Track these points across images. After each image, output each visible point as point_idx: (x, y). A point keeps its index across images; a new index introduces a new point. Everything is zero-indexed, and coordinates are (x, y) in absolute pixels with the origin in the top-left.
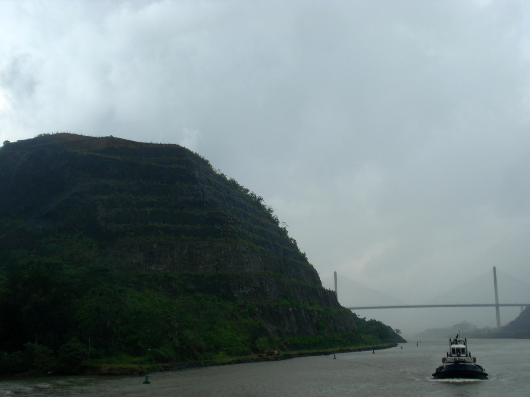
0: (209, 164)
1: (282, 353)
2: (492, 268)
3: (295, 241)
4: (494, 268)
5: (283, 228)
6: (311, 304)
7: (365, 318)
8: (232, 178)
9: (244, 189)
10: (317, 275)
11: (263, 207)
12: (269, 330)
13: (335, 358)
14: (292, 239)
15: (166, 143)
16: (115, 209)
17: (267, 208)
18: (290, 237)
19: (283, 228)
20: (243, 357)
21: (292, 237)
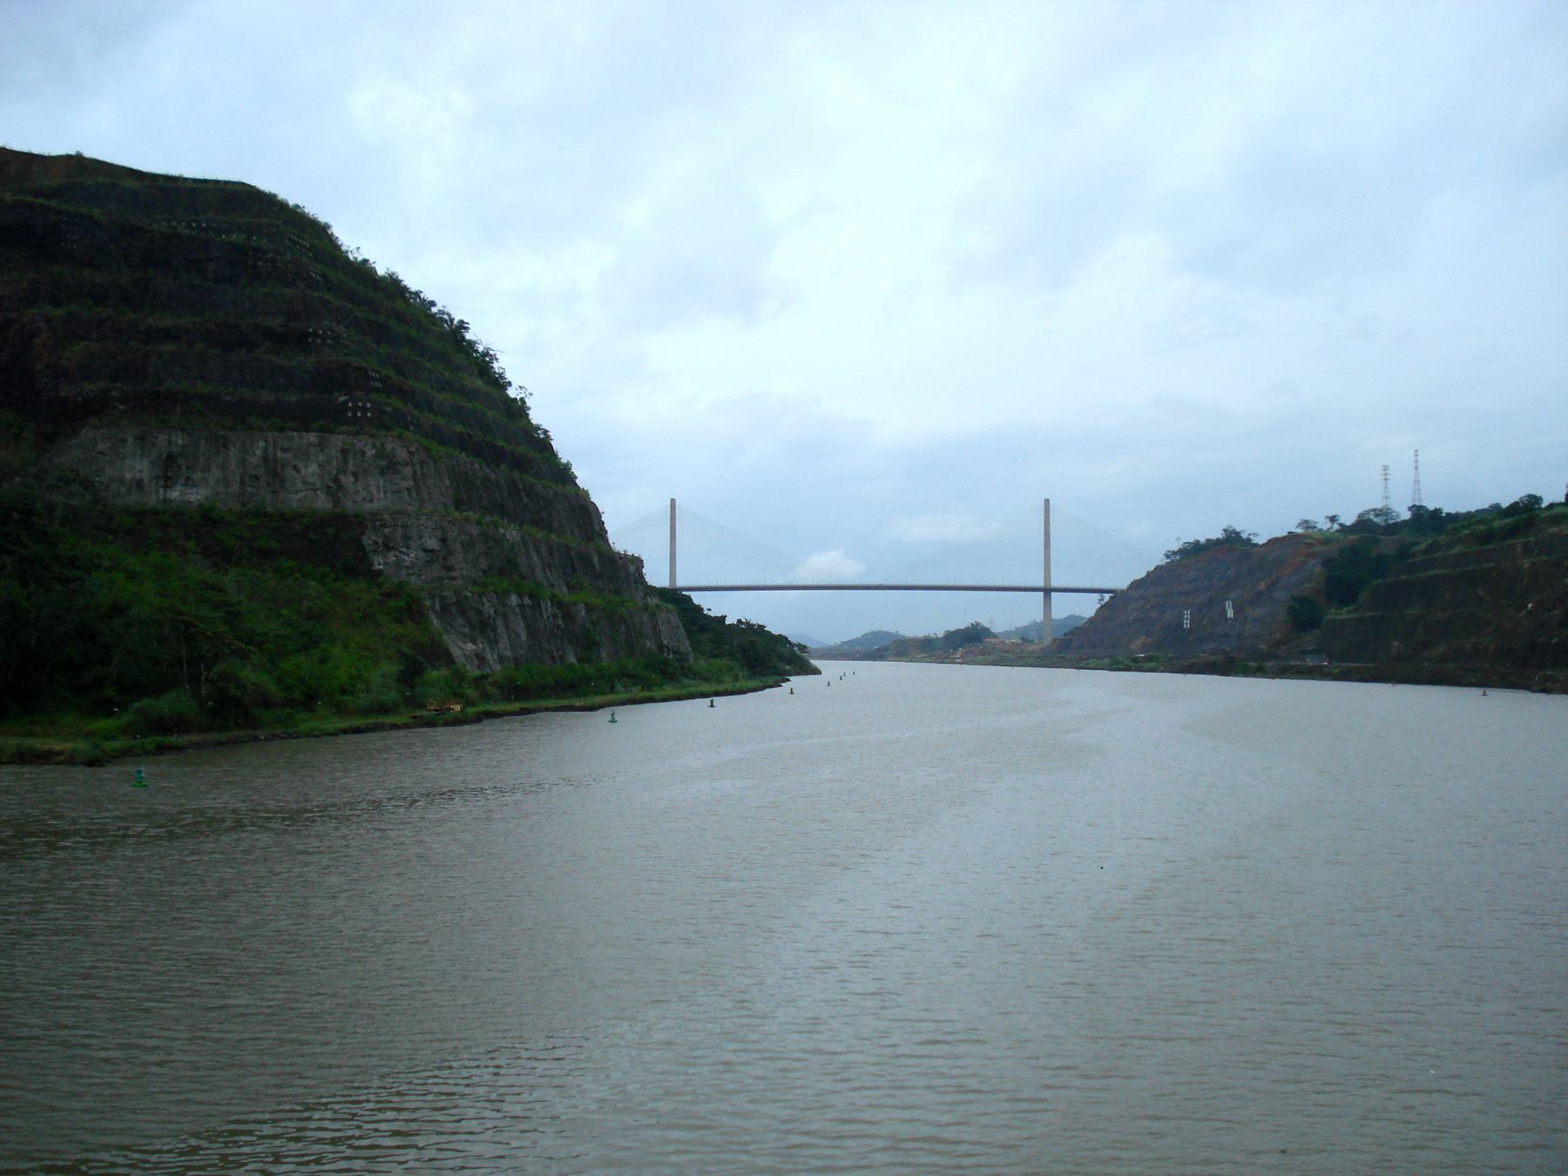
0: (332, 234)
3: (546, 432)
4: (673, 501)
5: (518, 399)
6: (571, 588)
8: (392, 270)
9: (424, 300)
10: (599, 515)
11: (471, 344)
13: (613, 721)
15: (219, 179)
16: (82, 344)
17: (481, 349)
18: (534, 422)
19: (518, 399)
21: (540, 423)
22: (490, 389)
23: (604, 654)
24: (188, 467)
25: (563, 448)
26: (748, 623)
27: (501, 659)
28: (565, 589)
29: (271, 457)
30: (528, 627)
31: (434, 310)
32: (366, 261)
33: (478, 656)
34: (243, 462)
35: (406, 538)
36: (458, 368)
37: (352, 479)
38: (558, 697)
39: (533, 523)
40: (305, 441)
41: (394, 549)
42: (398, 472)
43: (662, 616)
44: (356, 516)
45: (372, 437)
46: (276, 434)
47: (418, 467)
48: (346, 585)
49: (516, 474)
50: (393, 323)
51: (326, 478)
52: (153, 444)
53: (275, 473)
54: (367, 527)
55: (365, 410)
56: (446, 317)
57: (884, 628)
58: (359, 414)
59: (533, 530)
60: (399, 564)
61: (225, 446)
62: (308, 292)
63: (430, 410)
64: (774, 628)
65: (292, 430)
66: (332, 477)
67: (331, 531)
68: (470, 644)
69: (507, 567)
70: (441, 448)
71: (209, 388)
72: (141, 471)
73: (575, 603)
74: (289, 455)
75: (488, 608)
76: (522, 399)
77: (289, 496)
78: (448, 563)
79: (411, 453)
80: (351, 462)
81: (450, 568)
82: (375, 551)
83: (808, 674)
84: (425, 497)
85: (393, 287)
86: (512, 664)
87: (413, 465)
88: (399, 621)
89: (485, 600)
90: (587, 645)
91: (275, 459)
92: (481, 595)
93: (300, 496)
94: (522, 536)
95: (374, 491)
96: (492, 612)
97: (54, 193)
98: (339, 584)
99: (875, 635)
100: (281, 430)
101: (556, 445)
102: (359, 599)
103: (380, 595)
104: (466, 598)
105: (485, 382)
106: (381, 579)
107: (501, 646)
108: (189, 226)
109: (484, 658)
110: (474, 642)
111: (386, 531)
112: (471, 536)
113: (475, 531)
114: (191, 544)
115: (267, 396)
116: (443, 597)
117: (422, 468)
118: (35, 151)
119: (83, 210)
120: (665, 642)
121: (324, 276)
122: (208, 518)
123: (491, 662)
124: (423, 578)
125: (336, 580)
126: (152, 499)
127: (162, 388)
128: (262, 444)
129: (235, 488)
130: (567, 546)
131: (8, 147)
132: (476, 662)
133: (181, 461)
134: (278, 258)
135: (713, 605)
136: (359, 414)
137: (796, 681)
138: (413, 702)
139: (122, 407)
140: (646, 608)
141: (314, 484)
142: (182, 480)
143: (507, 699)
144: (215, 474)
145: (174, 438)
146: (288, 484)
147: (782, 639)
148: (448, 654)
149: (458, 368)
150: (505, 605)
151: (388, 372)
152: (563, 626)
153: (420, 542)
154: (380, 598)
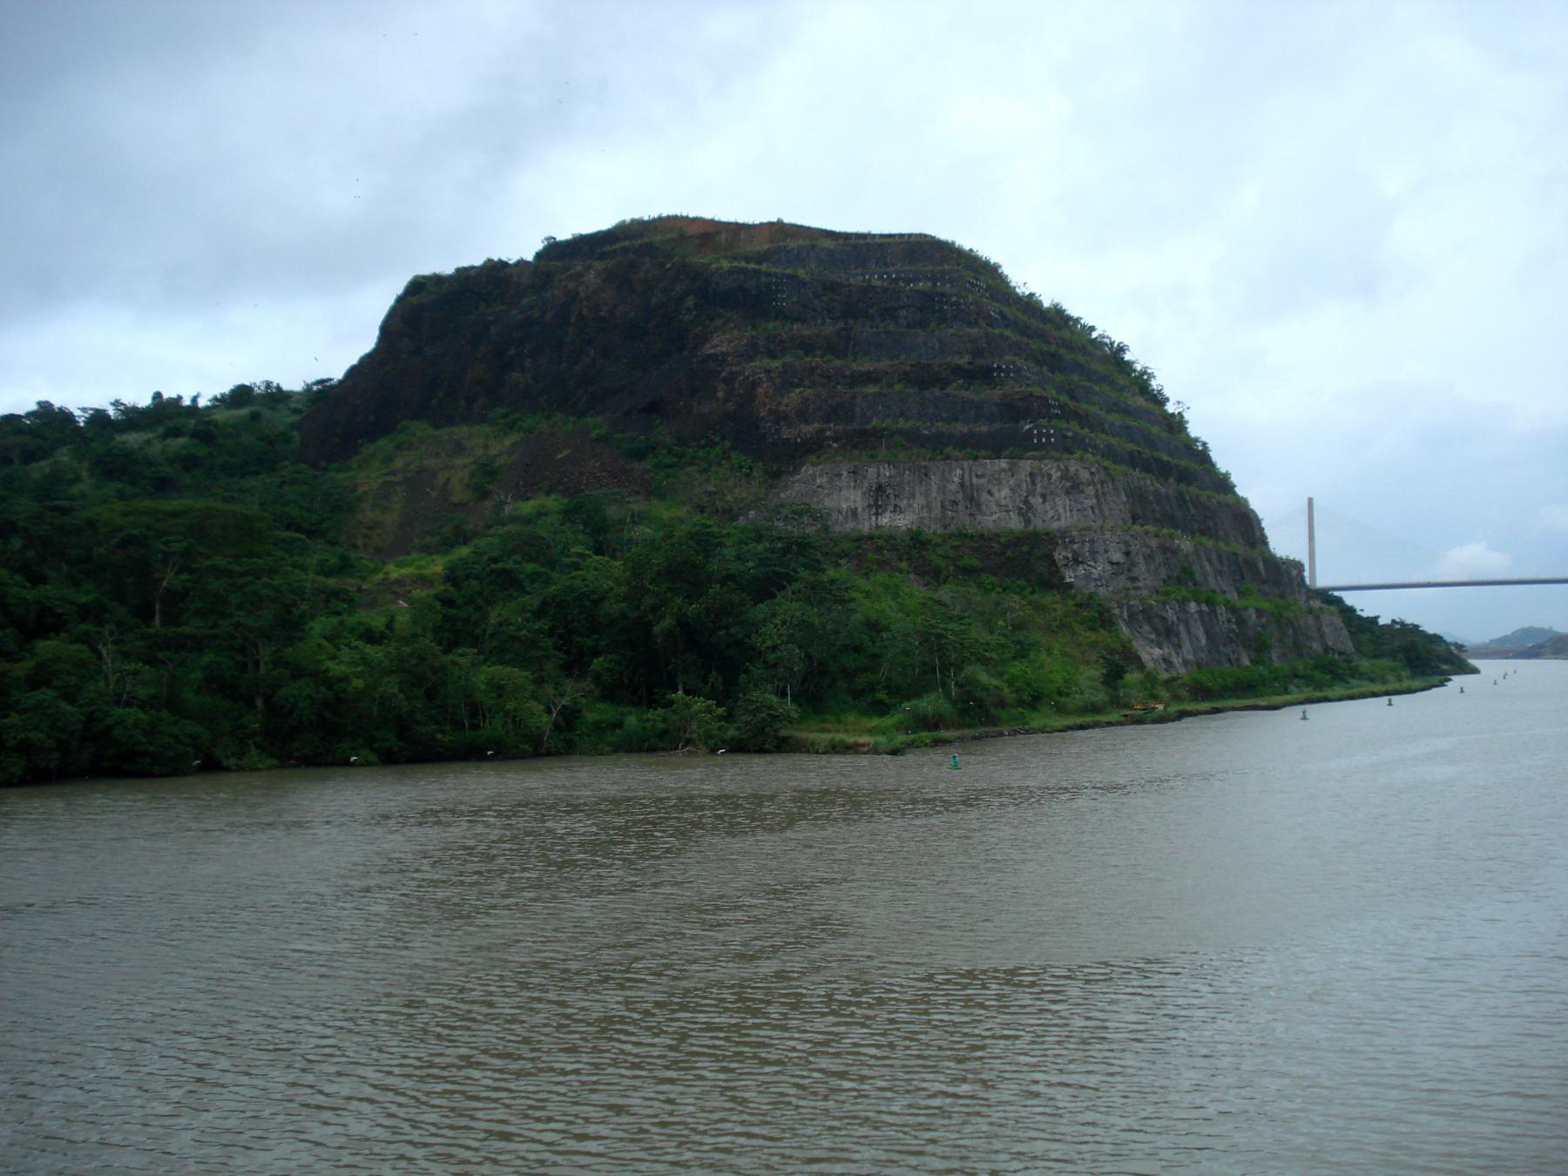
1: (1174, 708)
2: (1306, 503)
3: (1204, 444)
4: (1310, 501)
6: (1241, 594)
7: (1377, 617)
8: (1056, 301)
9: (1084, 326)
10: (1259, 522)
11: (1129, 364)
12: (1145, 657)
13: (1304, 718)
14: (1196, 440)
15: (904, 232)
16: (798, 391)
20: (1088, 719)
21: (1198, 436)
22: (1151, 406)
23: (1274, 656)
24: (896, 496)
25: (1223, 461)
26: (1402, 624)
27: (1186, 663)
28: (1235, 594)
29: (967, 484)
30: (1207, 633)
31: (1094, 335)
32: (1031, 295)
33: (1164, 660)
34: (942, 489)
35: (1093, 553)
36: (1122, 389)
37: (1041, 500)
38: (1238, 697)
39: (1203, 533)
40: (997, 468)
41: (1082, 563)
42: (1082, 492)
43: (1325, 619)
44: (1047, 534)
45: (1057, 460)
46: (971, 462)
47: (1099, 486)
48: (1043, 597)
49: (1183, 486)
50: (1062, 351)
51: (1018, 500)
52: (865, 477)
53: (972, 499)
54: (1057, 544)
55: (1049, 436)
56: (1107, 341)
57: (1538, 625)
58: (1044, 440)
59: (1205, 540)
60: (1088, 577)
61: (926, 475)
62: (990, 329)
63: (1103, 431)
64: (1429, 627)
65: (985, 458)
66: (1023, 499)
67: (1025, 548)
68: (1157, 649)
69: (1183, 576)
70: (1118, 467)
71: (910, 424)
72: (855, 501)
73: (1246, 608)
74: (983, 481)
75: (1171, 615)
76: (1179, 413)
77: (985, 517)
78: (1133, 575)
79: (1092, 473)
80: (1039, 486)
81: (1134, 579)
82: (1066, 565)
83: (1466, 673)
84: (1107, 513)
85: (1058, 317)
86: (1195, 667)
87: (1095, 485)
88: (1092, 629)
89: (1168, 608)
90: (1259, 648)
91: (971, 485)
92: (1164, 603)
93: (995, 517)
94: (1195, 546)
95: (1061, 510)
96: (1175, 618)
97: (761, 258)
98: (1036, 597)
99: (1527, 632)
100: (976, 458)
101: (1215, 456)
102: (1055, 610)
103: (1075, 605)
104: (1151, 607)
105: (1146, 400)
106: (1073, 591)
107: (1184, 650)
108: (881, 278)
109: (1170, 662)
110: (1161, 648)
111: (1075, 546)
112: (1151, 548)
113: (1154, 543)
114: (904, 565)
115: (960, 428)
116: (1130, 606)
117: (1103, 487)
118: (740, 221)
119: (789, 271)
120: (1330, 643)
121: (1002, 314)
122: (917, 541)
123: (1177, 665)
124: (1110, 589)
125: (1033, 593)
126: (866, 526)
127: (868, 427)
128: (959, 472)
129: (937, 512)
130: (1235, 554)
131: (716, 219)
132: (1164, 666)
133: (889, 491)
134: (962, 300)
135: (1365, 605)
136: (1044, 440)
137: (1457, 681)
138: (1116, 702)
139: (835, 445)
140: (1310, 611)
141: (1007, 506)
142: (891, 508)
143: (1196, 700)
144: (920, 500)
145: (882, 470)
146: (984, 507)
147: (1437, 639)
148: (1139, 658)
149: (1122, 389)
150: (1186, 612)
151: (1064, 399)
152: (1237, 631)
153: (1106, 556)
154: (1074, 609)
